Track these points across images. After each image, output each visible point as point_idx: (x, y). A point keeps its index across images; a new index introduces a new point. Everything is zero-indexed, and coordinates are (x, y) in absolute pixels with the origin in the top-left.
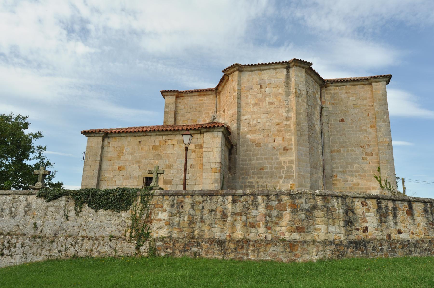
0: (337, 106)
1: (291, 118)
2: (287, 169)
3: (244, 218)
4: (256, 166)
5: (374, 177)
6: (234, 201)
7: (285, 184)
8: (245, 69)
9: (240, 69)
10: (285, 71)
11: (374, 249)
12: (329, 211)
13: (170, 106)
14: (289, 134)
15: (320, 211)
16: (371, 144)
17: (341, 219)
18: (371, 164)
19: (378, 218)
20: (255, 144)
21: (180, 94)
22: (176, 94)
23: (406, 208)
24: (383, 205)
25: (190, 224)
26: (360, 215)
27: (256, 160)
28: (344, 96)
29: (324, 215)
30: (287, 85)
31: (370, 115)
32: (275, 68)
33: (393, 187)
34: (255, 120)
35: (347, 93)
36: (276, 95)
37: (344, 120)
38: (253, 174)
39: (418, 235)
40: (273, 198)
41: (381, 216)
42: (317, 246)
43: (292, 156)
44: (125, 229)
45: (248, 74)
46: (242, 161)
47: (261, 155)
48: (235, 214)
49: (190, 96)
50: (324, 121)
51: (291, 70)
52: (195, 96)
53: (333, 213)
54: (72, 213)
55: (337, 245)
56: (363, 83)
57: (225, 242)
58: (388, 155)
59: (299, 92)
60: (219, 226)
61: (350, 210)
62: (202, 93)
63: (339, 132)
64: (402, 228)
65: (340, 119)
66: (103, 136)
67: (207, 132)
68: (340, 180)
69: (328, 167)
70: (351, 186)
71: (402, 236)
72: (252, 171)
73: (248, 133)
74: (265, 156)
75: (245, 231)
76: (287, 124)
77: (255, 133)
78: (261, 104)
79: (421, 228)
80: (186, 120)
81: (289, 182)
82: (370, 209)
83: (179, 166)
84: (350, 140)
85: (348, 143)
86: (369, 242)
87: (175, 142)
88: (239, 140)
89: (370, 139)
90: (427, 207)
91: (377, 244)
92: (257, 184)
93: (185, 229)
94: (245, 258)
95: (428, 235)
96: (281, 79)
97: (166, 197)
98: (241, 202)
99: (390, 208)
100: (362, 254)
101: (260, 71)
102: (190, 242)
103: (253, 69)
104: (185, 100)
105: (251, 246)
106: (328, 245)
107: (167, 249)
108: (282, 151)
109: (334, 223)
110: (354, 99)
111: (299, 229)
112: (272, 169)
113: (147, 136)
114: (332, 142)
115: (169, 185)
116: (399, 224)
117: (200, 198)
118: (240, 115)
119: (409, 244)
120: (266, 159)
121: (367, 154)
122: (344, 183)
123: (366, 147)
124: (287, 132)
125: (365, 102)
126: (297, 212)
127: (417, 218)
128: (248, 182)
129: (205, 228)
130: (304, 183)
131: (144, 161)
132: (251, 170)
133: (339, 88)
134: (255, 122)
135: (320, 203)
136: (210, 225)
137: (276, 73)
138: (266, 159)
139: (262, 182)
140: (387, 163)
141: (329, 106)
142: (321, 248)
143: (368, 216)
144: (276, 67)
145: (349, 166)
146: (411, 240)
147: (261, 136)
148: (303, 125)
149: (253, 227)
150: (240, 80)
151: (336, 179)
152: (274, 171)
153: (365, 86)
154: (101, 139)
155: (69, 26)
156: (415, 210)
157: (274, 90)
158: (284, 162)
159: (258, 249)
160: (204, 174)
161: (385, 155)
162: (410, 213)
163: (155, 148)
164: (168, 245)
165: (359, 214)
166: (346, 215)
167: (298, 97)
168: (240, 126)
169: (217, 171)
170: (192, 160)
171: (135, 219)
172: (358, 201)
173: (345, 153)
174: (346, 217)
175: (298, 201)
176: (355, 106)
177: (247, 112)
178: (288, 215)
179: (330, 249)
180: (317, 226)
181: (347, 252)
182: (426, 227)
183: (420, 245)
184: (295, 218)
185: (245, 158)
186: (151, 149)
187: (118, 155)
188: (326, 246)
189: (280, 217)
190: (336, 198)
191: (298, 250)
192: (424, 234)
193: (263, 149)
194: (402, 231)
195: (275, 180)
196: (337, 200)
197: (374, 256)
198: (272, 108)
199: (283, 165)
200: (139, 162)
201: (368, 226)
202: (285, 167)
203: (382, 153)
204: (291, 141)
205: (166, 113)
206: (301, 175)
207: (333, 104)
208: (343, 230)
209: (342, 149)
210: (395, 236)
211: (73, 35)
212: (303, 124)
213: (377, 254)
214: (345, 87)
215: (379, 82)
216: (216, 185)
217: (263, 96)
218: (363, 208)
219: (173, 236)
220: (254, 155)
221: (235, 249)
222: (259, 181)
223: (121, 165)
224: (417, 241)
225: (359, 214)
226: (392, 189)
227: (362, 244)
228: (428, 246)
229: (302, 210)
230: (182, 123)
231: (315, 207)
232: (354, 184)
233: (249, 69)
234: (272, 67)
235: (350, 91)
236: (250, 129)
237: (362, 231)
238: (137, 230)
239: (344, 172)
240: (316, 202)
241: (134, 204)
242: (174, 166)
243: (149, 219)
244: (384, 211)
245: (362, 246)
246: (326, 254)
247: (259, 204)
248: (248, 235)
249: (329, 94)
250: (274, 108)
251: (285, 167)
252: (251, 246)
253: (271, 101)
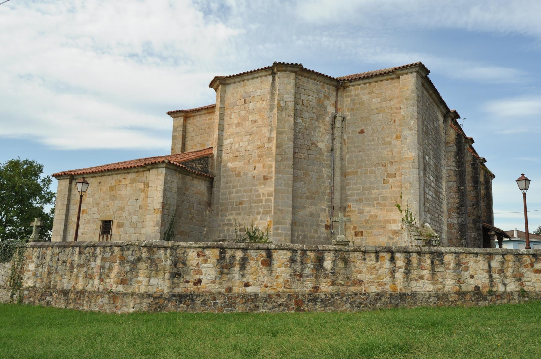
0: (357, 112)
1: (273, 138)
2: (265, 203)
3: (85, 269)
4: (235, 200)
5: (396, 205)
6: (80, 253)
7: (263, 221)
8: (228, 82)
9: (223, 82)
10: (270, 78)
11: (204, 303)
12: (153, 264)
13: (177, 130)
14: (270, 159)
15: (144, 263)
16: (394, 162)
17: (166, 272)
18: (393, 189)
19: (217, 269)
20: (235, 174)
21: (188, 113)
22: (183, 114)
23: (263, 257)
24: (228, 255)
25: (48, 275)
26: (193, 266)
27: (236, 193)
28: (366, 97)
29: (147, 267)
30: (271, 97)
31: (396, 122)
33: (414, 219)
34: (237, 144)
35: (370, 93)
36: (260, 111)
37: (365, 130)
38: (232, 210)
39: (274, 289)
40: (108, 249)
41: (222, 267)
42: (134, 298)
43: (270, 188)
44: (7, 278)
45: (233, 86)
46: (222, 194)
47: (240, 187)
48: (80, 266)
49: (199, 115)
50: (336, 135)
51: (277, 77)
52: (204, 114)
53: (158, 265)
55: (155, 298)
56: (389, 77)
57: (68, 293)
58: (412, 176)
59: (282, 104)
60: (68, 277)
61: (180, 262)
63: (357, 147)
64: (251, 281)
65: (359, 130)
66: (70, 179)
67: (152, 168)
68: (354, 211)
69: (337, 196)
70: (367, 218)
71: (249, 290)
72: (230, 207)
73: (229, 160)
74: (245, 188)
75: (85, 282)
76: (269, 146)
77: (235, 161)
78: (244, 123)
79: (281, 280)
80: (195, 145)
81: (266, 219)
82: (208, 259)
83: (130, 207)
84: (370, 158)
85: (367, 162)
86: (198, 296)
87: (128, 182)
88: (220, 169)
89: (394, 154)
90: (296, 256)
91: (209, 297)
92: (235, 222)
93: (45, 280)
94: (81, 308)
95: (290, 289)
96: (266, 90)
97: (35, 249)
98: (85, 254)
99: (238, 258)
100: (187, 308)
102: (45, 291)
103: (237, 80)
104: (195, 121)
105: (86, 297)
106: (145, 298)
107: (30, 298)
108: (262, 181)
109: (157, 276)
110: (378, 100)
111: (123, 282)
112: (250, 204)
113: (106, 175)
114: (348, 162)
116: (248, 276)
117: (56, 250)
118: (223, 139)
119: (256, 298)
120: (245, 191)
121: (389, 176)
122: (359, 215)
123: (389, 166)
124: (268, 157)
125: (392, 103)
126: (124, 264)
127: (277, 269)
128: (227, 220)
129: (58, 279)
130: (282, 219)
132: (230, 205)
133: (361, 88)
134: (237, 146)
135: (144, 255)
136: (61, 275)
137: (261, 82)
138: (245, 191)
139: (240, 219)
140: (410, 187)
141: (347, 113)
142: (138, 301)
143: (203, 268)
144: (260, 74)
145: (367, 192)
146: (261, 294)
147: (242, 164)
148: (286, 146)
149: (90, 279)
150: (224, 96)
151: (350, 210)
152: (252, 206)
153: (393, 81)
154: (68, 181)
155: (205, 6)
156: (276, 259)
157: (258, 105)
158: (263, 194)
159: (91, 300)
160: (148, 216)
161: (408, 176)
162: (268, 262)
163: (112, 188)
164: (31, 294)
165: (192, 265)
166: (174, 267)
167: (282, 111)
168: (222, 153)
169: (159, 212)
170: (141, 200)
171: (14, 270)
172: (193, 252)
173: (363, 176)
174: (174, 269)
175: (126, 253)
176: (379, 110)
177: (230, 134)
178: (117, 267)
179: (147, 301)
180: (140, 279)
181: (167, 306)
182: (289, 279)
183: (273, 300)
184: (122, 270)
185: (224, 191)
186: (108, 190)
188: (143, 299)
189: (110, 269)
190: (164, 249)
191: (119, 303)
192: (284, 287)
193: (243, 179)
194: (249, 284)
195: (253, 217)
196: (165, 251)
197: (203, 311)
198: (255, 128)
199: (261, 198)
201: (202, 279)
202: (264, 200)
203: (405, 174)
204: (272, 167)
205: (174, 138)
206: (279, 209)
207: (353, 110)
208: (167, 283)
209: (359, 170)
210: (238, 289)
211: (211, 17)
212: (285, 144)
213: (208, 308)
214: (368, 85)
215: (407, 73)
216: (157, 228)
217: (246, 113)
218: (199, 258)
219: (36, 286)
220: (234, 187)
221: (75, 299)
222: (237, 219)
224: (269, 295)
225: (192, 265)
226: (414, 222)
227: (188, 298)
228: (285, 301)
229: (128, 262)
230: (191, 148)
231: (139, 259)
232: (371, 216)
233: (232, 80)
234: (256, 75)
235: (374, 89)
236: (231, 155)
237: (192, 284)
238: (14, 280)
239: (360, 201)
240: (141, 253)
241: (14, 255)
242: (127, 208)
243: (22, 271)
244: (228, 261)
245: (188, 299)
246: (142, 307)
247: (97, 256)
248: (87, 286)
249: (349, 97)
250: (257, 127)
251: (264, 200)
252: (86, 297)
253: (254, 119)
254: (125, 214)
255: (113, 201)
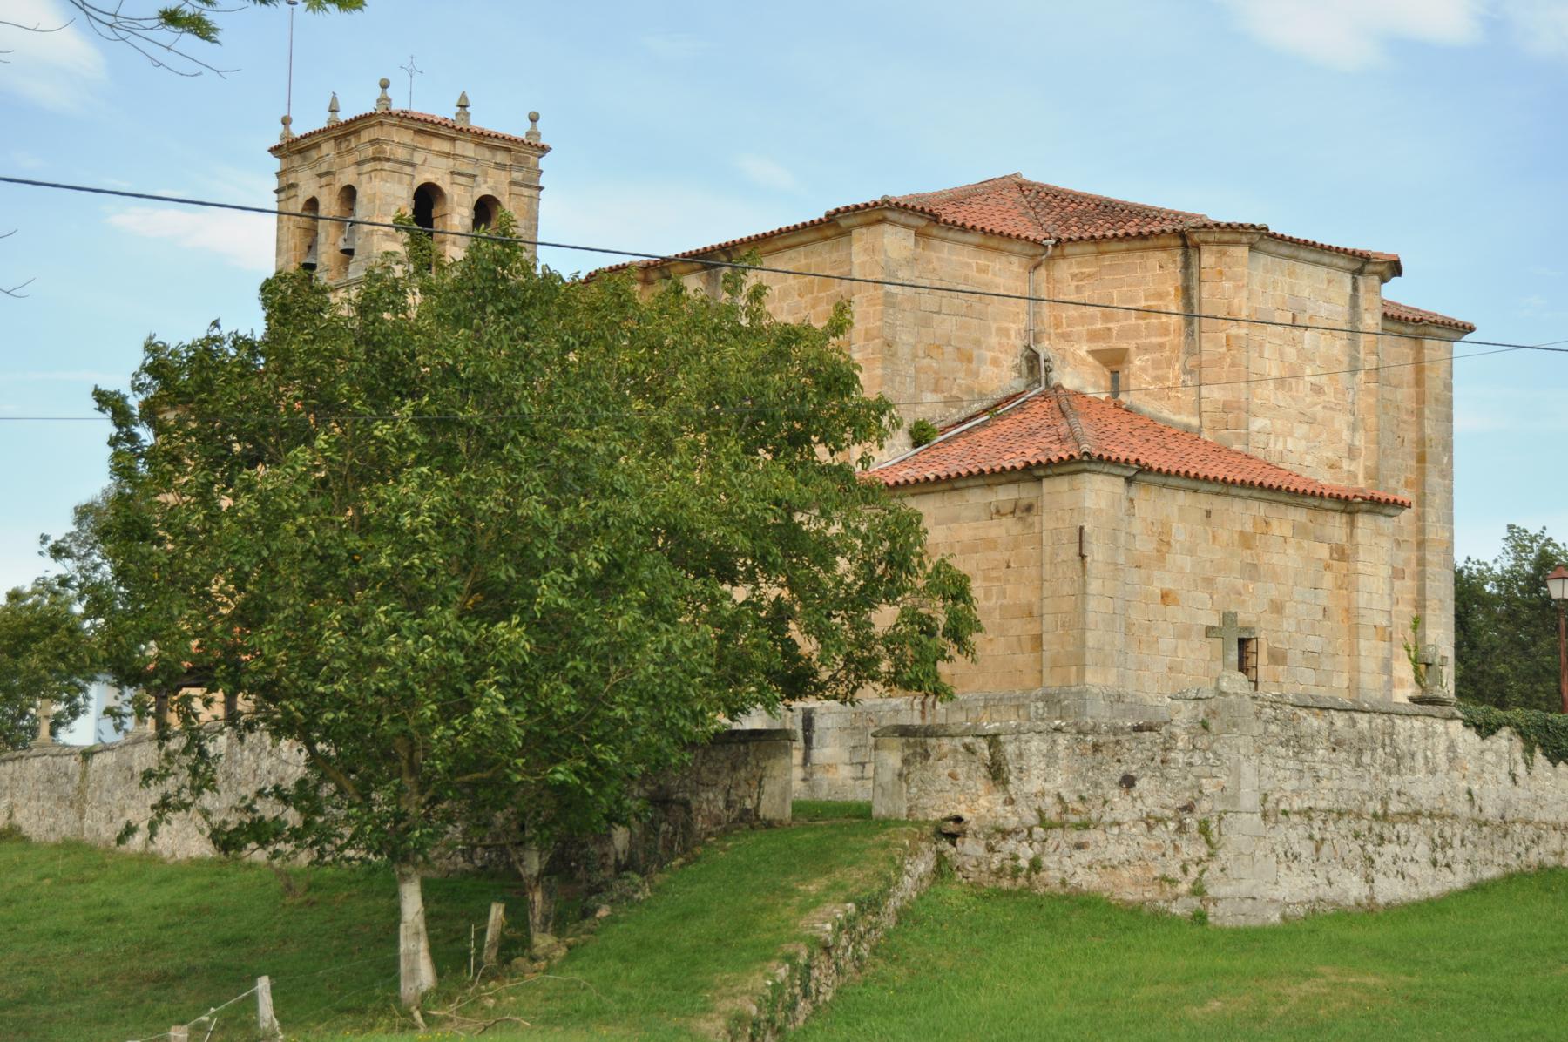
32: (1330, 266)
52: (965, 243)
54: (1521, 769)
62: (993, 243)
80: (939, 347)
83: (1299, 607)
101: (1291, 262)
115: (1281, 668)
131: (1220, 580)
144: (1335, 261)
186: (1236, 543)
187: (1158, 551)
198: (1318, 408)
200: (1209, 581)
223: (1168, 586)
234: (1326, 259)
250: (1324, 407)
254: (1289, 625)
255: (1251, 578)
